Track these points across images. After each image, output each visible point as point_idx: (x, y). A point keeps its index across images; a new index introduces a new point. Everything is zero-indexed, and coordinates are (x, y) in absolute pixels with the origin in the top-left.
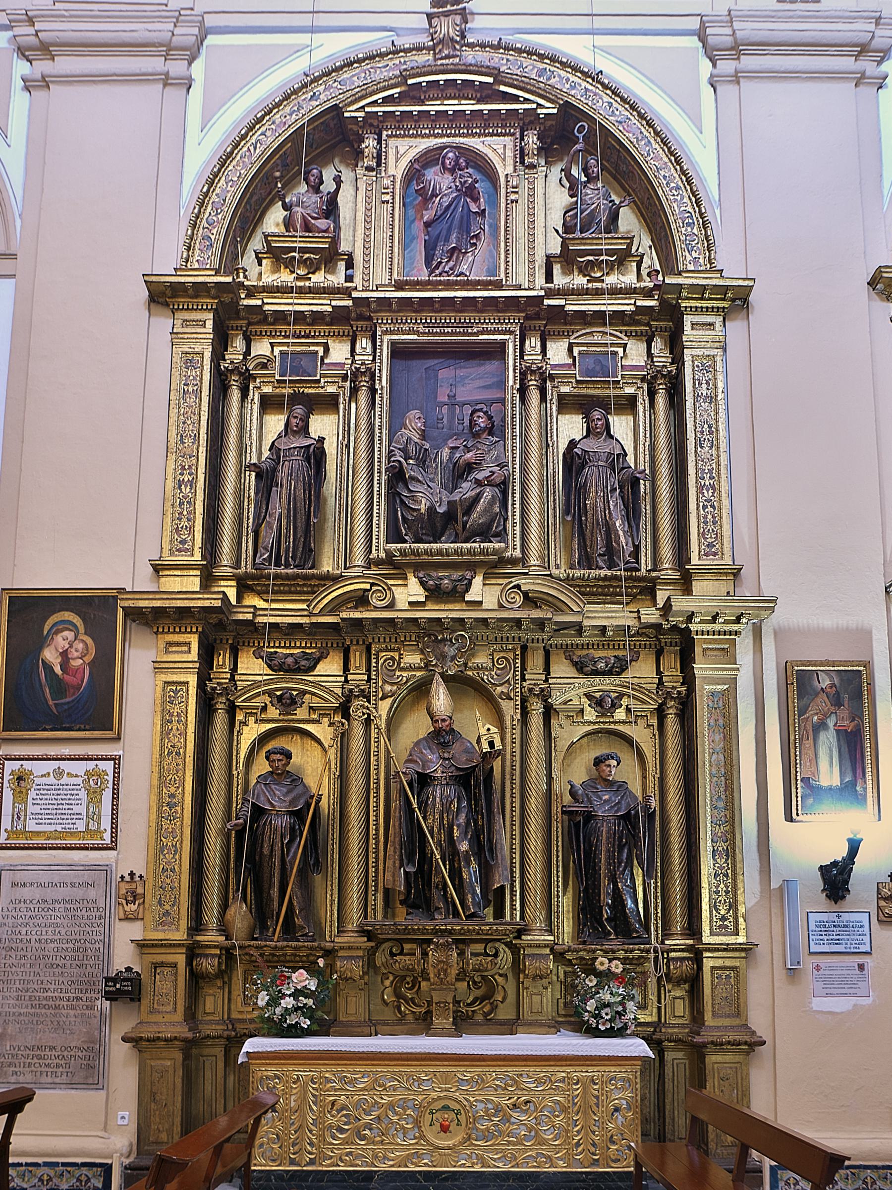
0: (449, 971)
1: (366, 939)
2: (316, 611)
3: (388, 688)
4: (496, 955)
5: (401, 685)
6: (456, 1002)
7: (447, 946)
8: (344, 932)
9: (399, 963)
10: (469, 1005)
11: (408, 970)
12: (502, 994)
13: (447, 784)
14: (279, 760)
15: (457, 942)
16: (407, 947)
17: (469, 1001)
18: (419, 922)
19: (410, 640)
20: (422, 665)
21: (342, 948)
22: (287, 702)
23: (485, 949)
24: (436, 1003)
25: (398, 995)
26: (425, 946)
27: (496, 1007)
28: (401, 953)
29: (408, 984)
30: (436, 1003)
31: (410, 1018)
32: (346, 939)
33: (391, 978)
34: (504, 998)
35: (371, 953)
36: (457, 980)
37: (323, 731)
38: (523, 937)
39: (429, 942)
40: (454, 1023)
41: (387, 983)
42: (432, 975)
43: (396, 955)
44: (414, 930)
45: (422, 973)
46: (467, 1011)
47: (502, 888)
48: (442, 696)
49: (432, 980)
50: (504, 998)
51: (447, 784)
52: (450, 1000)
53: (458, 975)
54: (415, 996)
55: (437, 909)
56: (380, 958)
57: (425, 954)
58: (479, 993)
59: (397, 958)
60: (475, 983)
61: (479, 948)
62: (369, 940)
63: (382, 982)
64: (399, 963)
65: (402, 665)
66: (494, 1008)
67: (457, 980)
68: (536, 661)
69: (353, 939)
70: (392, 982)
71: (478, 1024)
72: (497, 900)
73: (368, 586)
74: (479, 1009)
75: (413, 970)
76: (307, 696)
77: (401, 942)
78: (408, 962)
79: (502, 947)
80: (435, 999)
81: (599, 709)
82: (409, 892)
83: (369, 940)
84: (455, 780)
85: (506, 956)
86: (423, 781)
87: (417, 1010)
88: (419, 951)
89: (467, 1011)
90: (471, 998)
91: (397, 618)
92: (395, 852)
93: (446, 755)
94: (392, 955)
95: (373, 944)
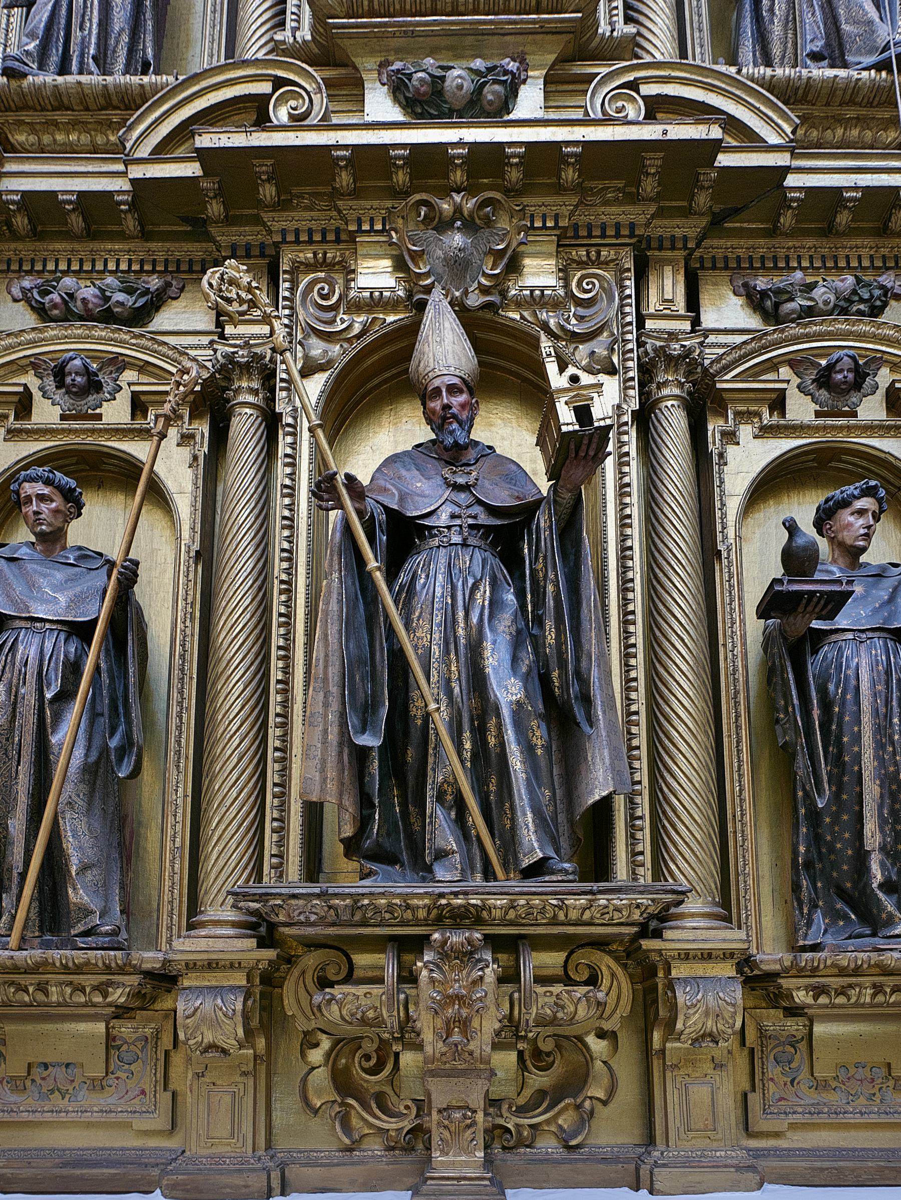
0: (475, 1023)
1: (253, 942)
2: (144, 152)
3: (317, 347)
4: (593, 981)
5: (349, 340)
6: (493, 1103)
7: (467, 955)
8: (202, 925)
9: (340, 1004)
10: (522, 1110)
11: (364, 1021)
12: (606, 1081)
13: (464, 545)
14: (42, 498)
15: (495, 943)
16: (362, 960)
17: (521, 1101)
18: (391, 889)
19: (372, 230)
20: (401, 293)
21: (192, 966)
22: (83, 386)
23: (565, 966)
24: (440, 1111)
25: (342, 1083)
26: (408, 958)
27: (592, 1113)
28: (349, 979)
29: (367, 1057)
30: (440, 1111)
31: (375, 1147)
32: (202, 944)
33: (326, 1044)
34: (612, 1091)
35: (268, 982)
36: (495, 1046)
37: (175, 467)
38: (668, 934)
39: (418, 944)
40: (488, 1162)
41: (316, 1056)
42: (428, 1036)
43: (331, 985)
44: (377, 910)
45: (402, 1029)
46: (517, 1126)
47: (605, 805)
48: (449, 336)
49: (429, 1049)
50: (612, 1091)
51: (464, 545)
52: (476, 1100)
53: (498, 1033)
54: (387, 1089)
55: (441, 855)
56: (292, 997)
57: (408, 977)
58: (538, 1080)
59: (338, 991)
60: (537, 1054)
61: (553, 960)
62: (260, 945)
63: (303, 1055)
64: (340, 1004)
65: (352, 294)
66: (586, 1118)
67: (495, 1046)
68: (668, 287)
69: (220, 944)
70: (328, 1055)
71: (546, 1160)
72: (590, 840)
73: (265, 88)
74: (548, 1122)
75: (378, 1022)
76: (129, 375)
77: (343, 947)
78: (363, 1001)
79: (606, 963)
80: (439, 1100)
81: (823, 394)
82: (363, 823)
83: (260, 945)
84: (485, 537)
85: (617, 988)
86: (403, 535)
87: (391, 1124)
88: (391, 972)
89: (517, 1126)
90: (527, 1093)
91: (338, 147)
92: (326, 705)
93: (461, 480)
94: (324, 983)
95: (270, 954)
